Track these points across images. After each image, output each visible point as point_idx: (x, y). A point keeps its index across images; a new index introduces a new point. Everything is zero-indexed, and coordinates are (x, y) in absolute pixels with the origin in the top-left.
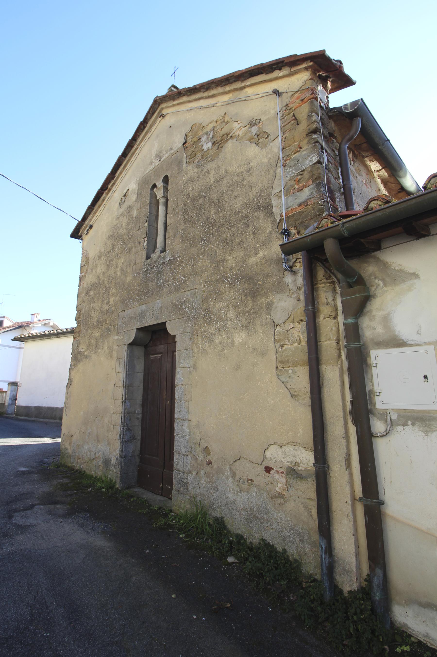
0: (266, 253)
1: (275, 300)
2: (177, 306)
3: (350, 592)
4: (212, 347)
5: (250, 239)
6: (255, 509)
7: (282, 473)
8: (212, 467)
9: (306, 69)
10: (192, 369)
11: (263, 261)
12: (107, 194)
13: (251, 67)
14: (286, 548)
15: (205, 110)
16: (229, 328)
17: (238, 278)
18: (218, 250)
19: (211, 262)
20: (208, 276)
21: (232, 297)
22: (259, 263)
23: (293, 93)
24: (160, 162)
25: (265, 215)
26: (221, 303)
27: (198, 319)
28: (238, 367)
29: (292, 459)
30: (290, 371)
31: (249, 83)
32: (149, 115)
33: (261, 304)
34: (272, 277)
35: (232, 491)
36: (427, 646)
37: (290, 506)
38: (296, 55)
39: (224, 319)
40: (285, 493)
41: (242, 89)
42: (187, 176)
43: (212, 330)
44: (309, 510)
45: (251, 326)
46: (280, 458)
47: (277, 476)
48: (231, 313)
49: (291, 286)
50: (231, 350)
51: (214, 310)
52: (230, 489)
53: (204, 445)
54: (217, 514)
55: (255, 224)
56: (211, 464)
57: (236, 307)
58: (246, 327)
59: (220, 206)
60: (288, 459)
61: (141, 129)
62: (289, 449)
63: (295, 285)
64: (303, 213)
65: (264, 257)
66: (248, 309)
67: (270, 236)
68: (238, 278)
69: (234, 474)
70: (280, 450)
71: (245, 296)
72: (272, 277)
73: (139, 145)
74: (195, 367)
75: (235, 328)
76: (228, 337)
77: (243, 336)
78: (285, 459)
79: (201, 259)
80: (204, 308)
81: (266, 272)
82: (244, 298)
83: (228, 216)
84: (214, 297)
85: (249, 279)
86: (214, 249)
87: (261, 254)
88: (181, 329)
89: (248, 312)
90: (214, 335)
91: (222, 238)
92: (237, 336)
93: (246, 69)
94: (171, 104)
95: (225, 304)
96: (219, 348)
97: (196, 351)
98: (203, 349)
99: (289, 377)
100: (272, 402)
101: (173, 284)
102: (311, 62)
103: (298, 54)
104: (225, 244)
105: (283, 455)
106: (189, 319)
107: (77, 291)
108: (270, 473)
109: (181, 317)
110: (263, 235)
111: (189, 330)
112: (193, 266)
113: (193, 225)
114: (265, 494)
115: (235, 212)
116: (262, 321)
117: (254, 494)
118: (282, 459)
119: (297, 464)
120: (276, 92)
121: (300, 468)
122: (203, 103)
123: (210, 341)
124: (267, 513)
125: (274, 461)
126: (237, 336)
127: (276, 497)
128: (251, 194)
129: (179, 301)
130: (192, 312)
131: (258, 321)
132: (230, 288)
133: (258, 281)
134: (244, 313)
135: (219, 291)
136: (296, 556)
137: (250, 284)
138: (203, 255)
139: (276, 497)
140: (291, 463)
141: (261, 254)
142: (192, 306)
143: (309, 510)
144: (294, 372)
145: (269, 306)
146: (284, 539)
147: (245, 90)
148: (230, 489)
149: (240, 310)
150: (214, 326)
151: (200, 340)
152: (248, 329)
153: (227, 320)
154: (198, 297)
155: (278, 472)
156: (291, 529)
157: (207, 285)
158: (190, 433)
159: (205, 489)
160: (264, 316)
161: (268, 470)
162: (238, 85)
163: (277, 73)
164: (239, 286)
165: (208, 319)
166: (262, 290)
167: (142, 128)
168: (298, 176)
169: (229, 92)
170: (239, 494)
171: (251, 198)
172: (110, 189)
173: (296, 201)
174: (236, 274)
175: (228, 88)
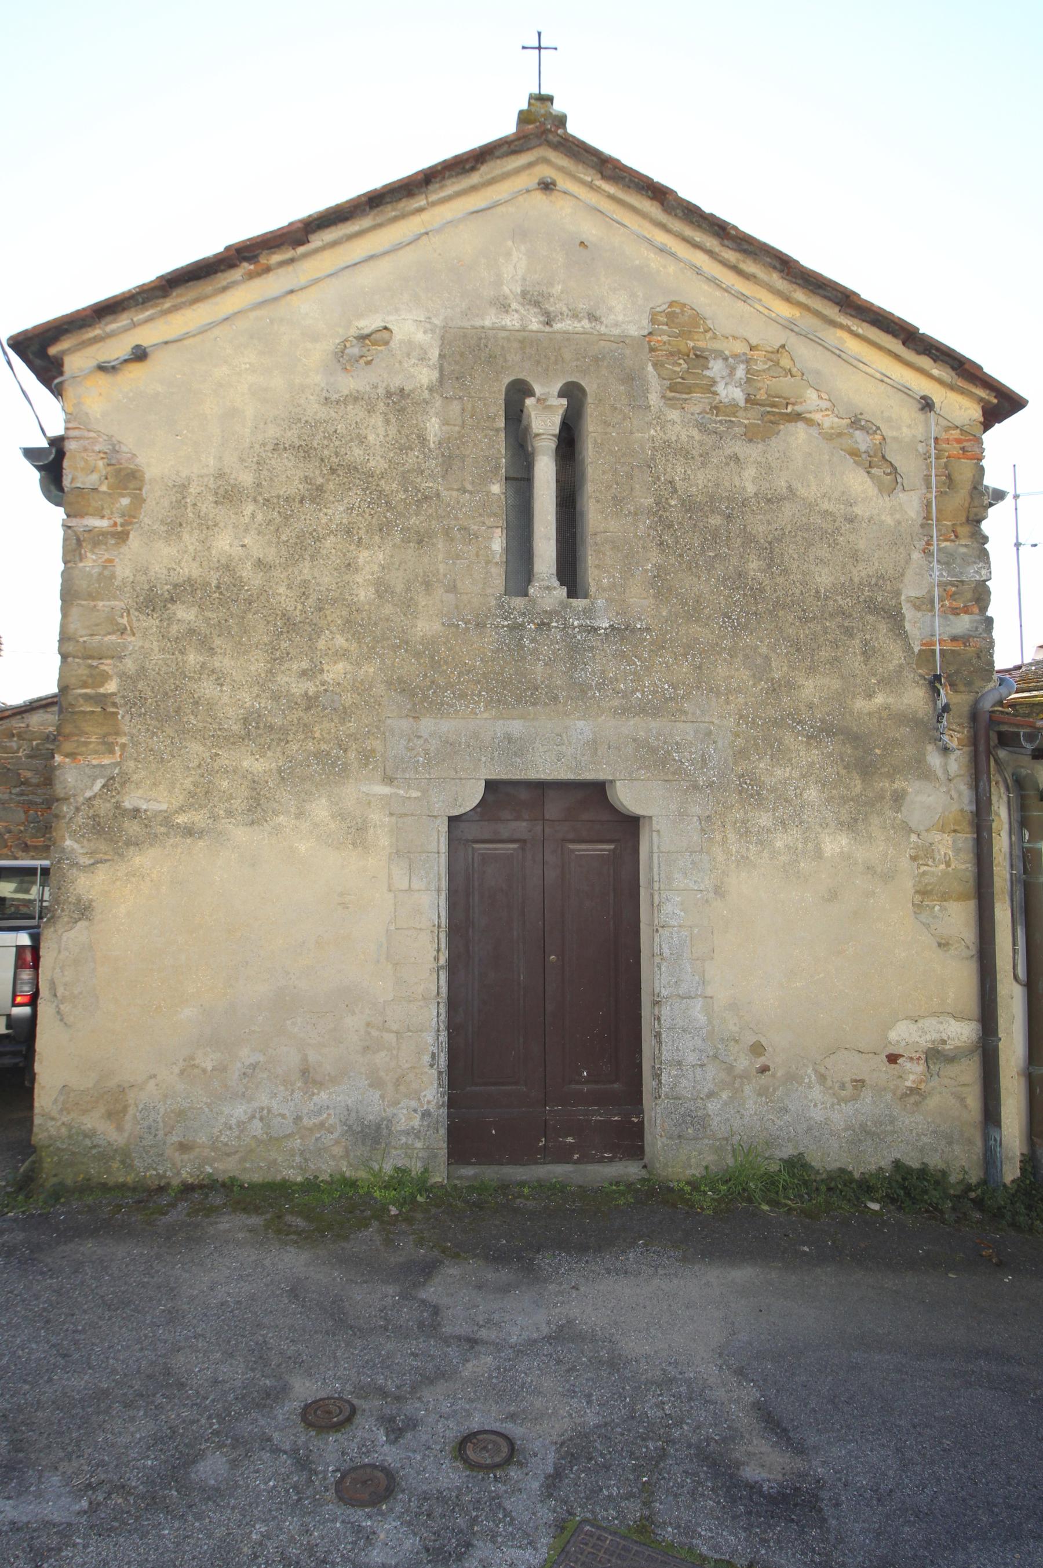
0: (891, 700)
1: (910, 790)
2: (653, 751)
3: (1013, 1181)
4: (765, 854)
5: (855, 662)
6: (869, 1123)
7: (919, 1059)
8: (773, 1076)
9: (981, 400)
10: (711, 895)
11: (885, 714)
12: (251, 276)
13: (872, 304)
14: (925, 1160)
15: (718, 293)
16: (808, 822)
17: (828, 730)
18: (773, 655)
19: (754, 675)
20: (746, 704)
21: (813, 763)
22: (876, 715)
23: (950, 425)
24: (547, 329)
25: (891, 630)
26: (788, 769)
27: (725, 791)
28: (833, 896)
29: (935, 1036)
30: (937, 908)
31: (860, 331)
32: (505, 148)
33: (882, 789)
34: (903, 747)
35: (820, 1106)
36: (450, 960)
37: (932, 1103)
38: (980, 368)
39: (794, 803)
40: (922, 1086)
41: (833, 323)
42: (665, 434)
43: (765, 819)
44: (962, 1100)
45: (860, 826)
46: (915, 1037)
47: (908, 1065)
48: (812, 794)
49: (940, 773)
50: (814, 864)
51: (769, 781)
52: (815, 1105)
53: (750, 1039)
54: (788, 1151)
55: (868, 637)
56: (769, 1070)
57: (824, 785)
58: (851, 825)
59: (777, 561)
60: (928, 1037)
61: (464, 168)
62: (930, 1023)
63: (946, 772)
64: (959, 655)
65: (887, 707)
66: (853, 794)
67: (901, 672)
68: (828, 730)
69: (822, 1078)
70: (913, 1027)
71: (845, 768)
72: (903, 747)
73: (434, 204)
74: (719, 891)
75: (824, 825)
76: (806, 840)
77: (844, 842)
78: (923, 1038)
79: (725, 660)
80: (739, 770)
81: (891, 735)
82: (843, 772)
83: (798, 592)
84: (766, 754)
85: (854, 738)
86: (764, 650)
87: (879, 699)
88: (673, 807)
89: (852, 800)
90: (769, 831)
91: (784, 635)
92: (827, 839)
93: (899, 318)
94: (589, 179)
95: (796, 774)
96: (783, 859)
97: (721, 857)
98: (742, 857)
99: (935, 917)
100: (903, 954)
101: (633, 692)
102: (995, 397)
103: (985, 370)
104: (792, 650)
105: (920, 1033)
106: (696, 787)
107: (58, 581)
108: (896, 1063)
109: (671, 777)
110: (885, 666)
111: (697, 810)
112: (700, 668)
113: (694, 570)
114: (889, 1096)
115: (817, 592)
116: (885, 822)
117: (868, 1100)
118: (918, 1039)
119: (944, 1042)
120: (927, 405)
121: (947, 1047)
122: (701, 259)
123: (760, 842)
124: (891, 1122)
125: (903, 1043)
126: (827, 839)
127: (906, 1095)
128: (855, 572)
129: (657, 739)
130: (704, 774)
131: (875, 820)
132: (808, 743)
133: (874, 748)
134: (844, 800)
135: (780, 743)
136: (941, 1166)
137: (856, 748)
138: (732, 652)
139: (906, 1095)
140: (933, 1042)
141: (879, 699)
142: (703, 760)
143: (962, 1100)
144: (943, 909)
145: (898, 799)
146: (921, 1150)
147: (832, 330)
148: (815, 1105)
149: (834, 792)
150: (770, 814)
151: (732, 837)
152: (853, 831)
153: (803, 807)
154: (720, 744)
155: (911, 1059)
156: (934, 1132)
157: (747, 725)
158: (710, 1022)
159: (755, 1118)
160: (889, 813)
161: (893, 1059)
162: (831, 311)
163: (925, 362)
164: (831, 746)
165: (752, 796)
166: (883, 765)
167: (467, 167)
168: (953, 585)
169: (799, 305)
170: (836, 1107)
171: (856, 580)
172: (268, 270)
173: (948, 629)
174: (822, 721)
175: (800, 295)
